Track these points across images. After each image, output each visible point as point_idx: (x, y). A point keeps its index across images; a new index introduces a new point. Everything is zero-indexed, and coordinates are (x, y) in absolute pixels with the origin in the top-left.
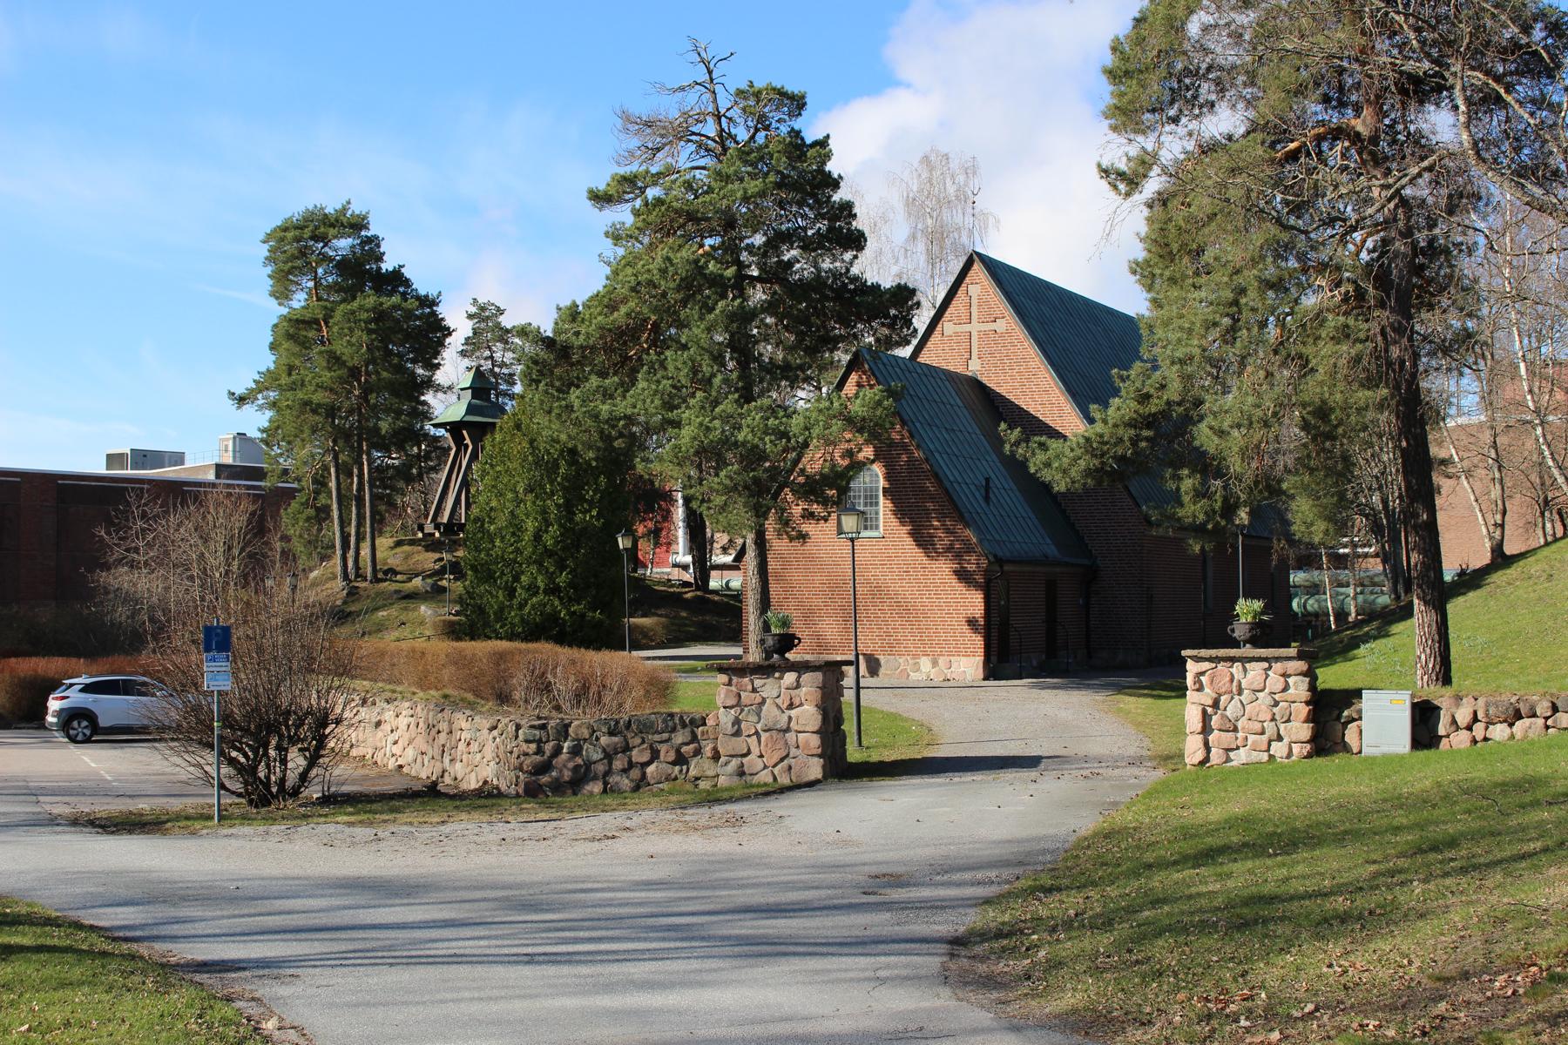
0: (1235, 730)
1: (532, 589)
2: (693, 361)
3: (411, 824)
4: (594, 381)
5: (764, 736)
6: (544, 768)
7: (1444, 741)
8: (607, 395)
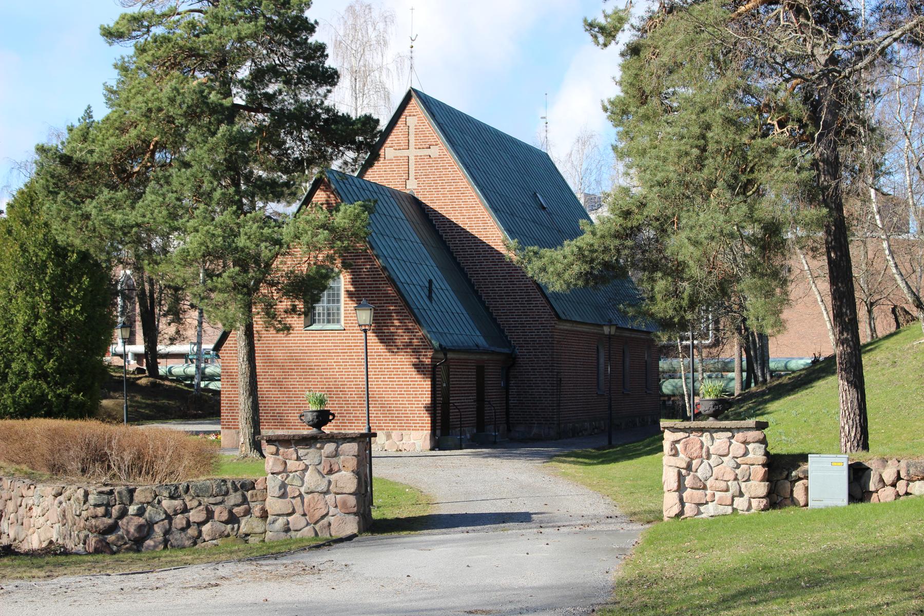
0: (705, 488)
1: (23, 375)
3: (21, 578)
4: (106, 194)
5: (307, 498)
6: (113, 528)
7: (875, 495)
8: (117, 207)
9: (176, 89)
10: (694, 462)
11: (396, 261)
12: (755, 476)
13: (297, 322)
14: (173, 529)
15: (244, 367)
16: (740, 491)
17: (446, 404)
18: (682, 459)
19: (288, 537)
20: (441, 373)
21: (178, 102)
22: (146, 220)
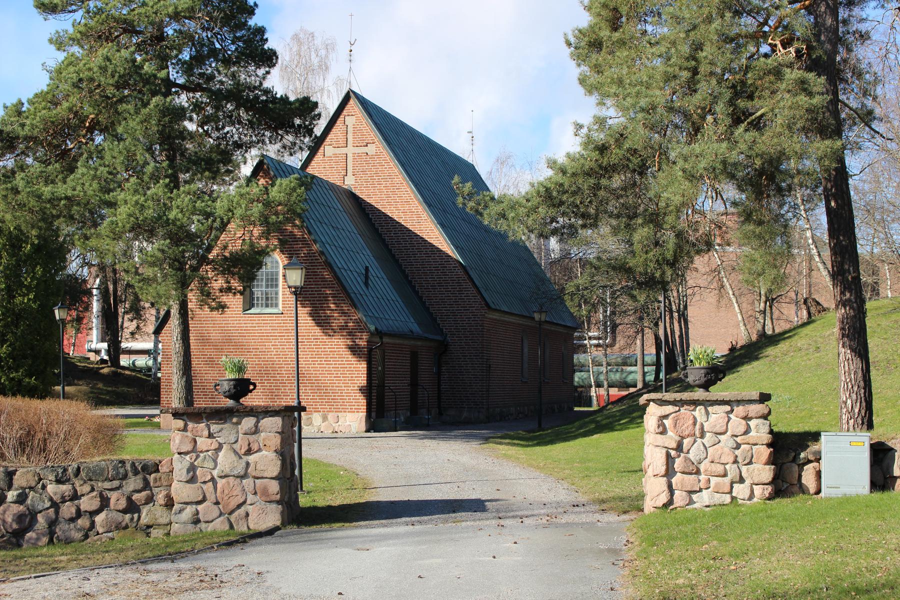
0: (698, 472)
2: (128, 151)
5: (221, 483)
8: (49, 181)
9: (108, 59)
10: (685, 441)
11: (333, 248)
12: (758, 458)
13: (235, 302)
14: (61, 519)
15: (177, 346)
16: (741, 477)
17: (382, 386)
18: (671, 438)
19: (198, 530)
20: (377, 355)
21: (110, 71)
22: (76, 193)
